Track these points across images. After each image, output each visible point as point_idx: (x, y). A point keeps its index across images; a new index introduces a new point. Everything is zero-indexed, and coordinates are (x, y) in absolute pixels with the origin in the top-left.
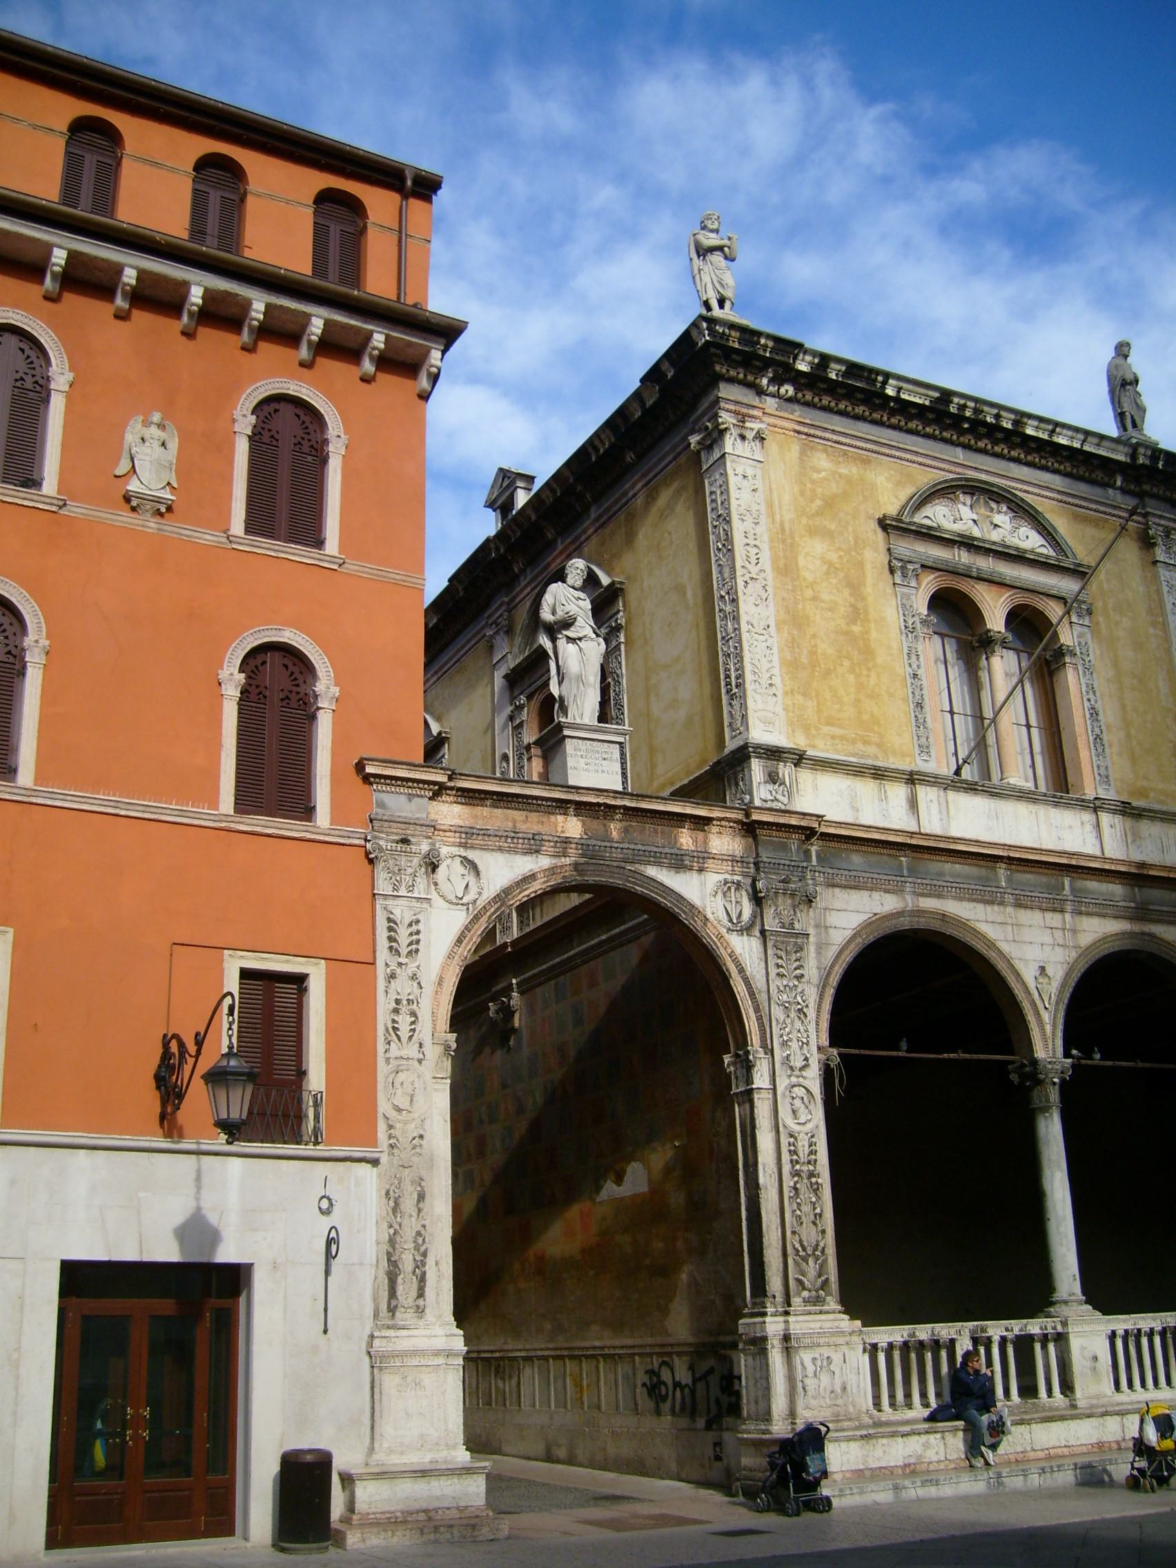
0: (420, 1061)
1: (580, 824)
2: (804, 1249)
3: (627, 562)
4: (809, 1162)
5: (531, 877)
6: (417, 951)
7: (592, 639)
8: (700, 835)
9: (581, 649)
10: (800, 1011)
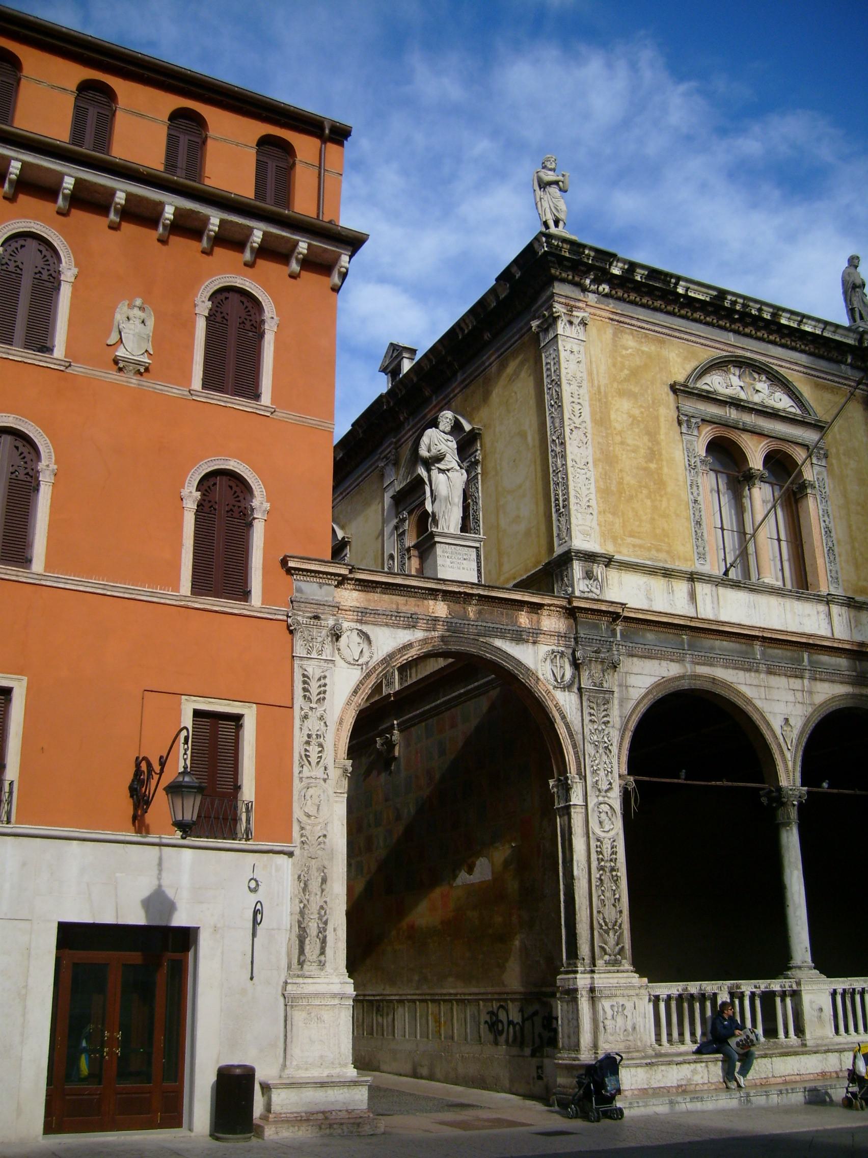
0: (325, 780)
1: (446, 607)
2: (606, 924)
3: (484, 413)
4: (611, 860)
5: (409, 646)
6: (324, 699)
7: (457, 471)
8: (535, 617)
9: (448, 478)
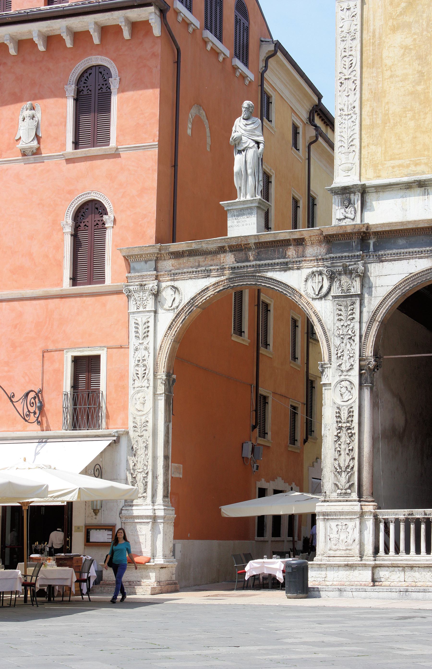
0: (148, 387)
1: (233, 256)
2: (340, 468)
4: (348, 422)
5: (207, 289)
6: (147, 336)
8: (300, 248)
10: (350, 338)
